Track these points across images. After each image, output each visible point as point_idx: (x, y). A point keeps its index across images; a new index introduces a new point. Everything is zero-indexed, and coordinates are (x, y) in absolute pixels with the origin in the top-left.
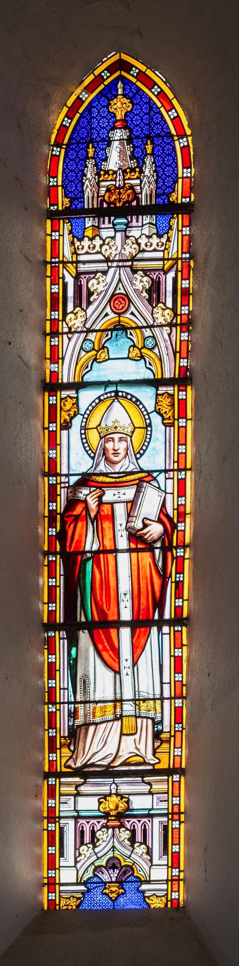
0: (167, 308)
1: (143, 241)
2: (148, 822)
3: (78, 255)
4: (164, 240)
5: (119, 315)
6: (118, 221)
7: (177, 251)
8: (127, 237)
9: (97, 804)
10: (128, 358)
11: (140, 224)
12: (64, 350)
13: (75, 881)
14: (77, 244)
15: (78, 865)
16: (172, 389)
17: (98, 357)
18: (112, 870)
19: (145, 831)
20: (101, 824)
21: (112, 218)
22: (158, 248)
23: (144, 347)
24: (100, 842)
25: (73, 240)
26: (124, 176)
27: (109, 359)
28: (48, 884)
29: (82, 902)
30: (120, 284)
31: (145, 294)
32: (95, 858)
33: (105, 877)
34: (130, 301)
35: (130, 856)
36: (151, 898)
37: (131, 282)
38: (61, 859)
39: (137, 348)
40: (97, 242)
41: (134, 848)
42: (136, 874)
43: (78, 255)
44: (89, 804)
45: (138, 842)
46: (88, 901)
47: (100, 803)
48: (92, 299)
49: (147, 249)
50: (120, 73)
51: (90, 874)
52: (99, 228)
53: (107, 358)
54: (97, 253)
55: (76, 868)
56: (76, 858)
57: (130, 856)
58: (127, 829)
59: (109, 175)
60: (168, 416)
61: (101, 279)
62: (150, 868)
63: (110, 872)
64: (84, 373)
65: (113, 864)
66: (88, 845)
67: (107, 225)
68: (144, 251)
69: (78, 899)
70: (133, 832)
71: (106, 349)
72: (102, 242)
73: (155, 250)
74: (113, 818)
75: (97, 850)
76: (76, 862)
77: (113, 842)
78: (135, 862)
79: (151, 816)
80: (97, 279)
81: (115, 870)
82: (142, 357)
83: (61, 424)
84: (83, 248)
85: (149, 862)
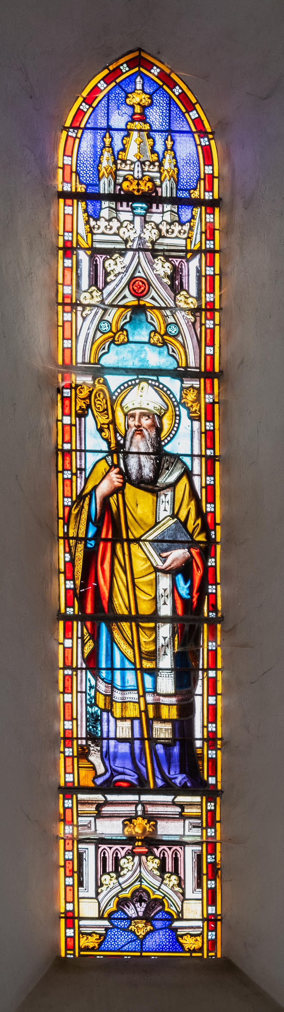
0: (191, 296)
1: (164, 228)
2: (179, 850)
3: (93, 234)
4: (186, 228)
5: (139, 298)
6: (135, 205)
7: (201, 241)
8: (146, 222)
9: (121, 826)
10: (149, 343)
11: (160, 210)
12: (79, 328)
13: (97, 916)
14: (92, 223)
15: (100, 897)
16: (198, 383)
17: (116, 339)
18: (139, 904)
19: (176, 860)
20: (125, 850)
21: (130, 203)
22: (180, 236)
23: (166, 333)
24: (125, 871)
25: (89, 219)
26: (142, 168)
27: (128, 342)
28: (66, 918)
29: (105, 938)
30: (140, 267)
31: (166, 280)
32: (118, 889)
33: (131, 912)
34: (150, 285)
35: (159, 887)
36: (185, 937)
37: (151, 266)
38: (80, 888)
39: (159, 334)
40: (115, 224)
41: (163, 879)
42: (166, 909)
43: (93, 234)
44: (111, 828)
45: (169, 872)
46: (111, 938)
47: (125, 826)
48: (108, 279)
49: (168, 236)
50: (139, 69)
51: (113, 907)
52: (116, 210)
53: (126, 340)
54: (115, 234)
55: (98, 900)
56: (97, 887)
57: (159, 887)
58: (156, 857)
59: (126, 164)
60: (194, 410)
61: (118, 260)
62: (182, 902)
63: (136, 905)
64: (100, 354)
65: (139, 896)
66: (111, 874)
67: (125, 207)
68: (164, 237)
69: (101, 935)
70: (163, 861)
71: (125, 333)
72: (119, 224)
73: (177, 237)
74: (140, 844)
75: (121, 880)
76: (97, 894)
77: (140, 872)
78: (165, 896)
79: (182, 844)
80: (114, 260)
81: (143, 904)
82: (165, 343)
83: (76, 411)
84: (99, 228)
85: (181, 896)
